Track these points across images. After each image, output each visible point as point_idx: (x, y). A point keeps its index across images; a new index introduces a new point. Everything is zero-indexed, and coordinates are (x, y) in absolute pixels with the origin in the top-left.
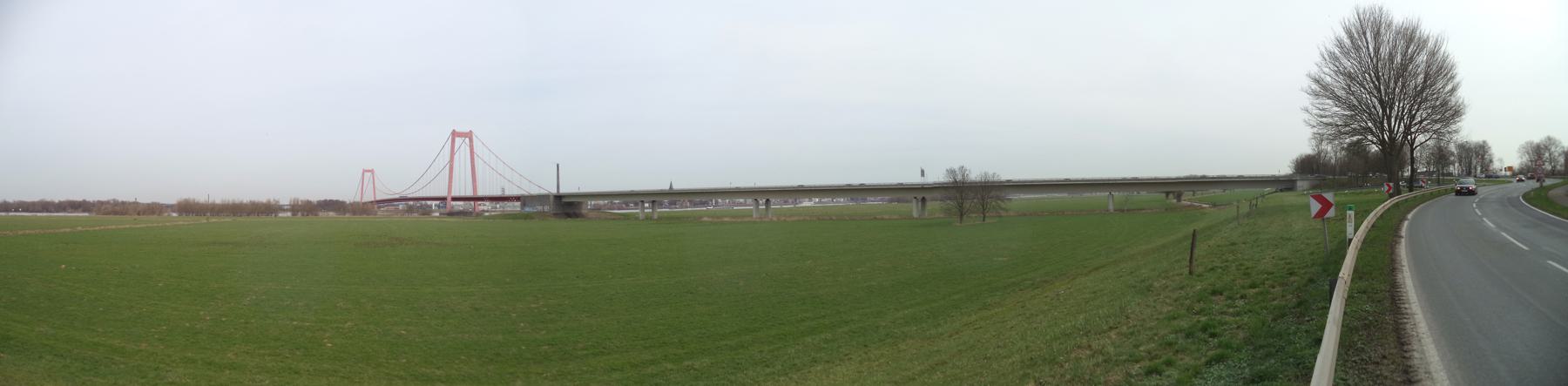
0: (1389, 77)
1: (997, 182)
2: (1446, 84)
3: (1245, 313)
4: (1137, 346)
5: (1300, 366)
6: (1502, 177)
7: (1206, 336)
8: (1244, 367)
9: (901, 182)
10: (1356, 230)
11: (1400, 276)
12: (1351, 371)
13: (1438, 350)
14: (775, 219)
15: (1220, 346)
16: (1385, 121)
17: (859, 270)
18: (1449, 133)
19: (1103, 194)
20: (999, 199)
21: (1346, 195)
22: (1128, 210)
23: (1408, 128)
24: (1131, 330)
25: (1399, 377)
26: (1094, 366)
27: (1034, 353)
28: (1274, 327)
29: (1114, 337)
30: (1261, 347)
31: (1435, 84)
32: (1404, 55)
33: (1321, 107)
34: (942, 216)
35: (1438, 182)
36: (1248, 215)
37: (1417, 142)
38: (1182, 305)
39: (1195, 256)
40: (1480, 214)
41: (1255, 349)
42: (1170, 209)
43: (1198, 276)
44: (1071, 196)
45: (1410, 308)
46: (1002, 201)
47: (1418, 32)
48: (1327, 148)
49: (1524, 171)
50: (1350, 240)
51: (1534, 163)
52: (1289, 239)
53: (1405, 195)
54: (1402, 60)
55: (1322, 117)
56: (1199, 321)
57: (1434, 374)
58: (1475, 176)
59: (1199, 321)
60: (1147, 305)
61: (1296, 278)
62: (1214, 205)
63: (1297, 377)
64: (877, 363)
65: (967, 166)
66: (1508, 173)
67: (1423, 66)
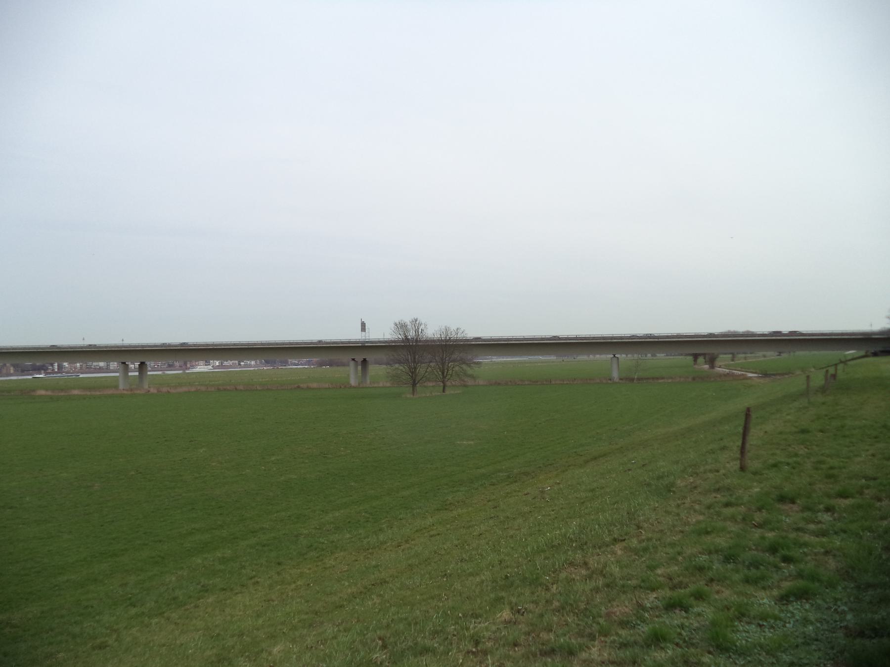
3: (836, 533)
4: (652, 568)
7: (778, 559)
8: (844, 612)
9: (320, 339)
14: (153, 390)
15: (800, 575)
17: (273, 458)
19: (604, 357)
20: (464, 363)
22: (639, 379)
24: (644, 544)
26: (591, 590)
27: (509, 570)
29: (619, 552)
30: (869, 586)
34: (388, 384)
36: (823, 390)
38: (719, 514)
42: (699, 378)
44: (560, 359)
46: (469, 365)
56: (763, 538)
59: (763, 538)
60: (666, 512)
62: (765, 375)
64: (293, 586)
65: (422, 319)
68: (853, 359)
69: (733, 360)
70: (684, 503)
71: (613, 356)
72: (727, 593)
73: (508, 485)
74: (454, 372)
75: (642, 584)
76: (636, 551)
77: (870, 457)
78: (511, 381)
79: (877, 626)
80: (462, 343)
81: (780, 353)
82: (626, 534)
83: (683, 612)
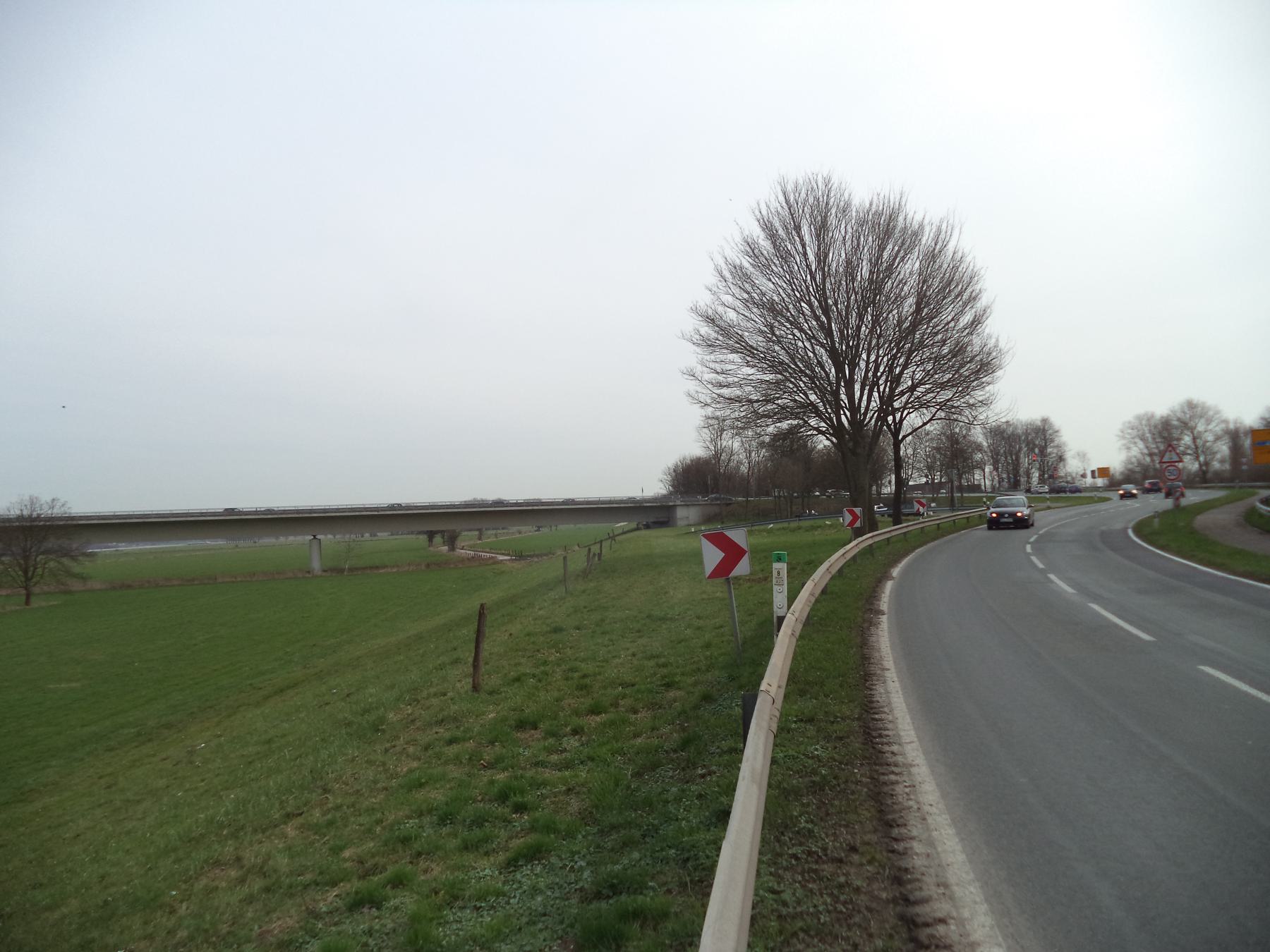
0: (848, 307)
1: (60, 519)
2: (962, 312)
4: (336, 850)
5: (690, 864)
6: (1086, 489)
7: (507, 810)
8: (581, 869)
10: (791, 600)
11: (880, 689)
12: (788, 875)
13: (962, 840)
15: (533, 829)
16: (843, 390)
18: (971, 406)
19: (300, 539)
20: (65, 555)
21: (772, 534)
22: (351, 570)
23: (887, 401)
25: (885, 889)
26: (240, 901)
27: (113, 890)
28: (638, 789)
30: (614, 827)
31: (938, 313)
32: (875, 263)
33: (718, 367)
35: (952, 504)
36: (585, 574)
37: (906, 428)
38: (438, 756)
39: (484, 654)
40: (1041, 566)
41: (601, 832)
43: (491, 693)
44: (232, 544)
45: (903, 754)
46: (74, 558)
47: (901, 218)
48: (733, 443)
49: (1138, 476)
50: (781, 620)
51: (1157, 459)
52: (663, 619)
53: (886, 531)
54: (871, 272)
55: (721, 386)
56: (492, 782)
57: (955, 888)
58: (1028, 491)
59: (492, 782)
61: (679, 693)
62: (520, 556)
63: (683, 885)
66: (1100, 482)
67: (913, 281)
68: (624, 533)
69: (480, 539)
70: (394, 746)
71: (312, 537)
72: (437, 870)
73: (136, 747)
74: (46, 570)
75: (319, 879)
76: (316, 829)
77: (630, 658)
78: (149, 582)
79: (615, 881)
80: (61, 523)
81: (539, 527)
82: (305, 805)
83: (374, 909)
